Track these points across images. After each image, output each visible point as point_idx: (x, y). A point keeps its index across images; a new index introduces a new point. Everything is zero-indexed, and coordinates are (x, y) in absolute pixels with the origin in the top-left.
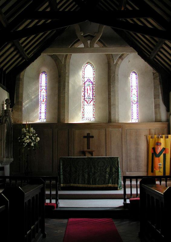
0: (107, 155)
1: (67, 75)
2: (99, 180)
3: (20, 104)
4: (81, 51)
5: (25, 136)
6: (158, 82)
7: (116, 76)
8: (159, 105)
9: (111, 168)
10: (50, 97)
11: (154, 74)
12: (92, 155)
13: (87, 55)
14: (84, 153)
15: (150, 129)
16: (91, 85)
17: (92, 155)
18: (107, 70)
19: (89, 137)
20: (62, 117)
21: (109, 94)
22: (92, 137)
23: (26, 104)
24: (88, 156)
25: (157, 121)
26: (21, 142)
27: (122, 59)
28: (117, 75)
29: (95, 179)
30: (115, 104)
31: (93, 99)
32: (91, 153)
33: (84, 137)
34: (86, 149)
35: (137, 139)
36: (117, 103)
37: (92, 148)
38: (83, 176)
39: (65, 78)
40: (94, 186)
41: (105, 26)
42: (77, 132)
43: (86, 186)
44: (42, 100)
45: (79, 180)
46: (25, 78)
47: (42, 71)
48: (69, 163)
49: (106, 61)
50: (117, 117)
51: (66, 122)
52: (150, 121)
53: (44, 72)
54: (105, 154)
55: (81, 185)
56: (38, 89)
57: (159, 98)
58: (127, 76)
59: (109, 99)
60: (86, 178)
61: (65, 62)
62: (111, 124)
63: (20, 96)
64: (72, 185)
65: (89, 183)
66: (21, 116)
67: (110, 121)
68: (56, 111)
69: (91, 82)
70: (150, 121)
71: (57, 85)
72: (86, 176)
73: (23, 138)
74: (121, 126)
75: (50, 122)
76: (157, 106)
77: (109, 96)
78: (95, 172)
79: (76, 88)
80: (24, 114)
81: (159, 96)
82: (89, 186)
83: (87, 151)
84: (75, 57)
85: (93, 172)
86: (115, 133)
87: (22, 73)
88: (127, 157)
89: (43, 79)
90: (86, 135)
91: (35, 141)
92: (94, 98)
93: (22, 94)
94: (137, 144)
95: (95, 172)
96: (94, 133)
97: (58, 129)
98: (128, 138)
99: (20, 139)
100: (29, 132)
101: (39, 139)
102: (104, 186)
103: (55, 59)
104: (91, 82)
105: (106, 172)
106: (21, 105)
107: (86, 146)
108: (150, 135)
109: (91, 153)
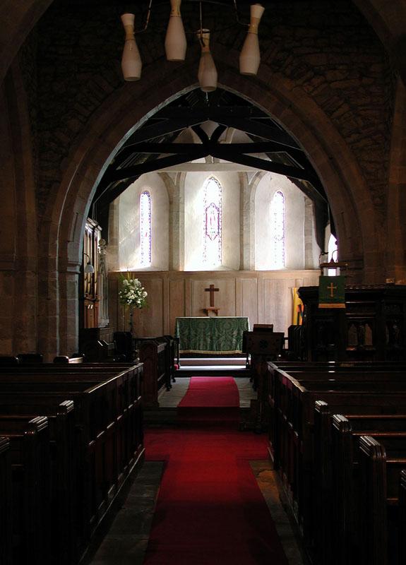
0: (186, 314)
1: (181, 200)
2: (224, 345)
3: (115, 242)
4: (201, 168)
5: (129, 291)
6: (311, 211)
7: (251, 202)
8: (311, 244)
9: (239, 330)
10: (157, 231)
11: (305, 199)
12: (217, 314)
13: (211, 174)
14: (205, 312)
15: (296, 280)
16: (216, 212)
17: (217, 314)
18: (239, 192)
19: (212, 290)
20: (175, 262)
21: (241, 229)
22: (217, 290)
23: (123, 241)
24: (211, 315)
25: (307, 268)
26: (123, 298)
27: (261, 178)
28: (253, 201)
29: (220, 345)
30: (248, 244)
31: (218, 233)
32: (216, 312)
33: (207, 290)
34: (208, 307)
35: (278, 293)
36: (251, 242)
37: (217, 305)
38: (205, 340)
39: (179, 207)
40: (218, 353)
41: (235, 129)
42: (196, 283)
43: (209, 352)
44: (144, 235)
45: (199, 345)
46: (120, 205)
47: (143, 191)
48: (188, 324)
49: (238, 179)
50: (251, 262)
51: (181, 270)
52: (298, 268)
53: (146, 193)
54: (183, 314)
55: (202, 352)
56: (139, 210)
57: (311, 235)
58: (267, 201)
59: (241, 236)
60: (209, 342)
61: (178, 182)
62: (243, 272)
63: (115, 231)
64: (191, 351)
65: (212, 349)
66: (117, 260)
67: (241, 268)
68: (167, 252)
69: (216, 208)
70: (298, 268)
71: (167, 215)
72: (209, 340)
73: (127, 294)
74: (256, 275)
75: (157, 268)
76: (308, 247)
77: (241, 232)
78: (219, 335)
79: (195, 218)
80: (121, 255)
81: (311, 231)
82: (212, 352)
83: (210, 310)
84: (191, 176)
85: (217, 335)
86: (248, 284)
87: (115, 202)
88: (264, 318)
89: (145, 200)
90: (209, 287)
91: (142, 297)
92: (220, 231)
93: (117, 228)
94: (278, 300)
95: (219, 335)
96: (219, 284)
97: (167, 279)
98: (266, 292)
99: (121, 294)
100: (133, 284)
101: (146, 293)
102: (230, 352)
103: (165, 177)
104: (216, 208)
105: (232, 336)
106: (117, 244)
107: (208, 301)
108: (296, 287)
109: (216, 312)
